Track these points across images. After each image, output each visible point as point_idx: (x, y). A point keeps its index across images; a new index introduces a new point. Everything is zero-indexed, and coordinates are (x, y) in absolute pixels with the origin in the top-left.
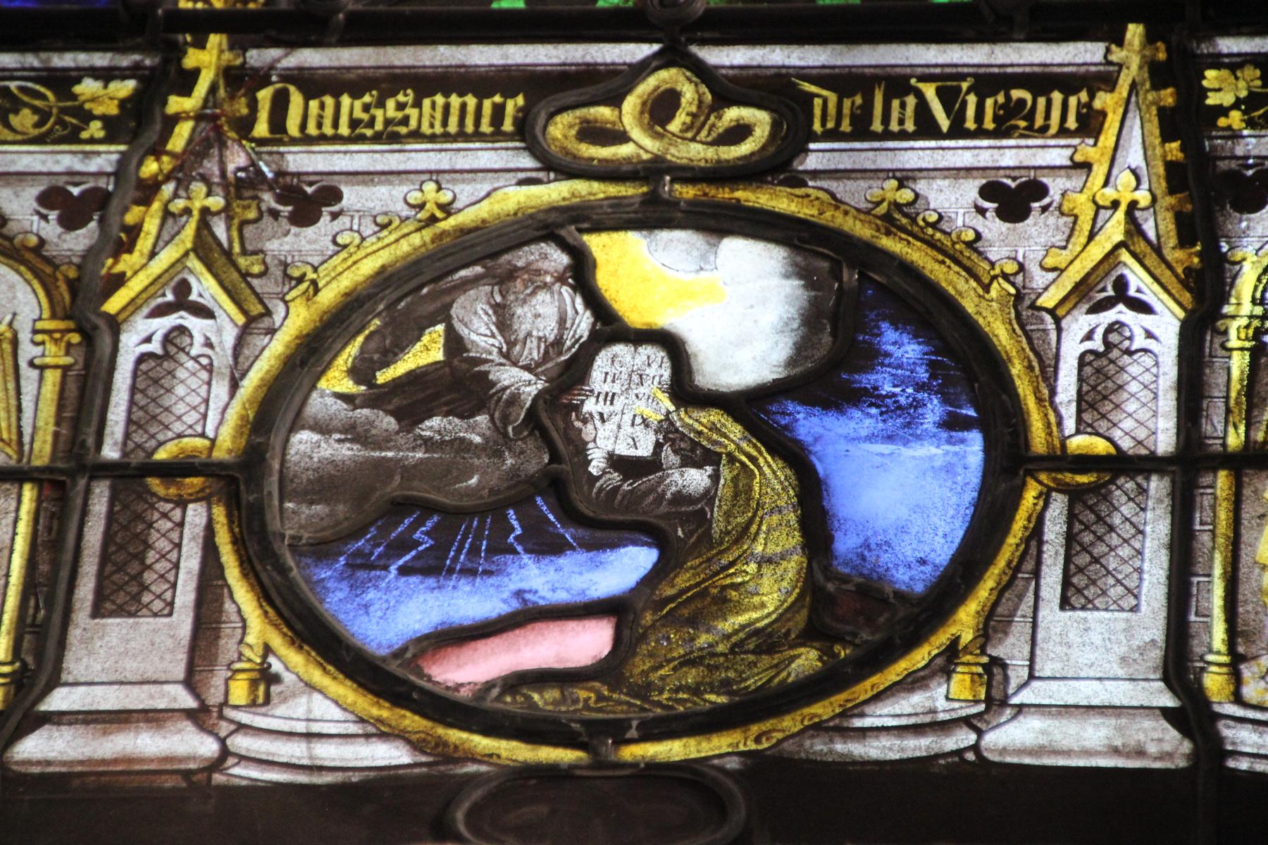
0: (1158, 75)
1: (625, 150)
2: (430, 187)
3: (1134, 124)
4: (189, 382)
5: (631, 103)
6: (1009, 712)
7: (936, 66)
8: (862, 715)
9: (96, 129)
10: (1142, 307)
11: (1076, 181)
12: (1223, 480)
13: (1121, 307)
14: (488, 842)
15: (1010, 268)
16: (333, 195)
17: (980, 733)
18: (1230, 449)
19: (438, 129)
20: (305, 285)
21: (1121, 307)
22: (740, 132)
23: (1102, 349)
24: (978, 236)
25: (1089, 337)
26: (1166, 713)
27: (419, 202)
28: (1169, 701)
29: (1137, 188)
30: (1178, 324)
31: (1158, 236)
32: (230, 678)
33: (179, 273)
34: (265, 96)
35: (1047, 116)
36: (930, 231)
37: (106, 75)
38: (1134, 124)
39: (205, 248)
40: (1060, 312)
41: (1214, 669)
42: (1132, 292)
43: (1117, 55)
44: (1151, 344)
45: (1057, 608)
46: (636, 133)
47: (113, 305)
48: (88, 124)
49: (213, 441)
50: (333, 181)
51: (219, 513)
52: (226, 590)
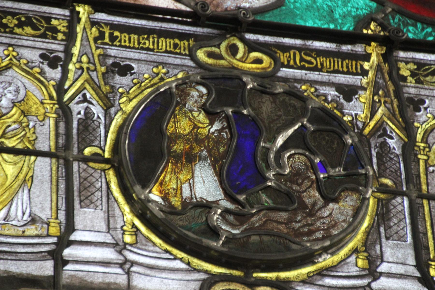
1: (222, 62)
7: (106, 20)
8: (333, 271)
14: (34, 287)
22: (258, 61)
34: (292, 52)
35: (162, 46)
50: (424, 98)
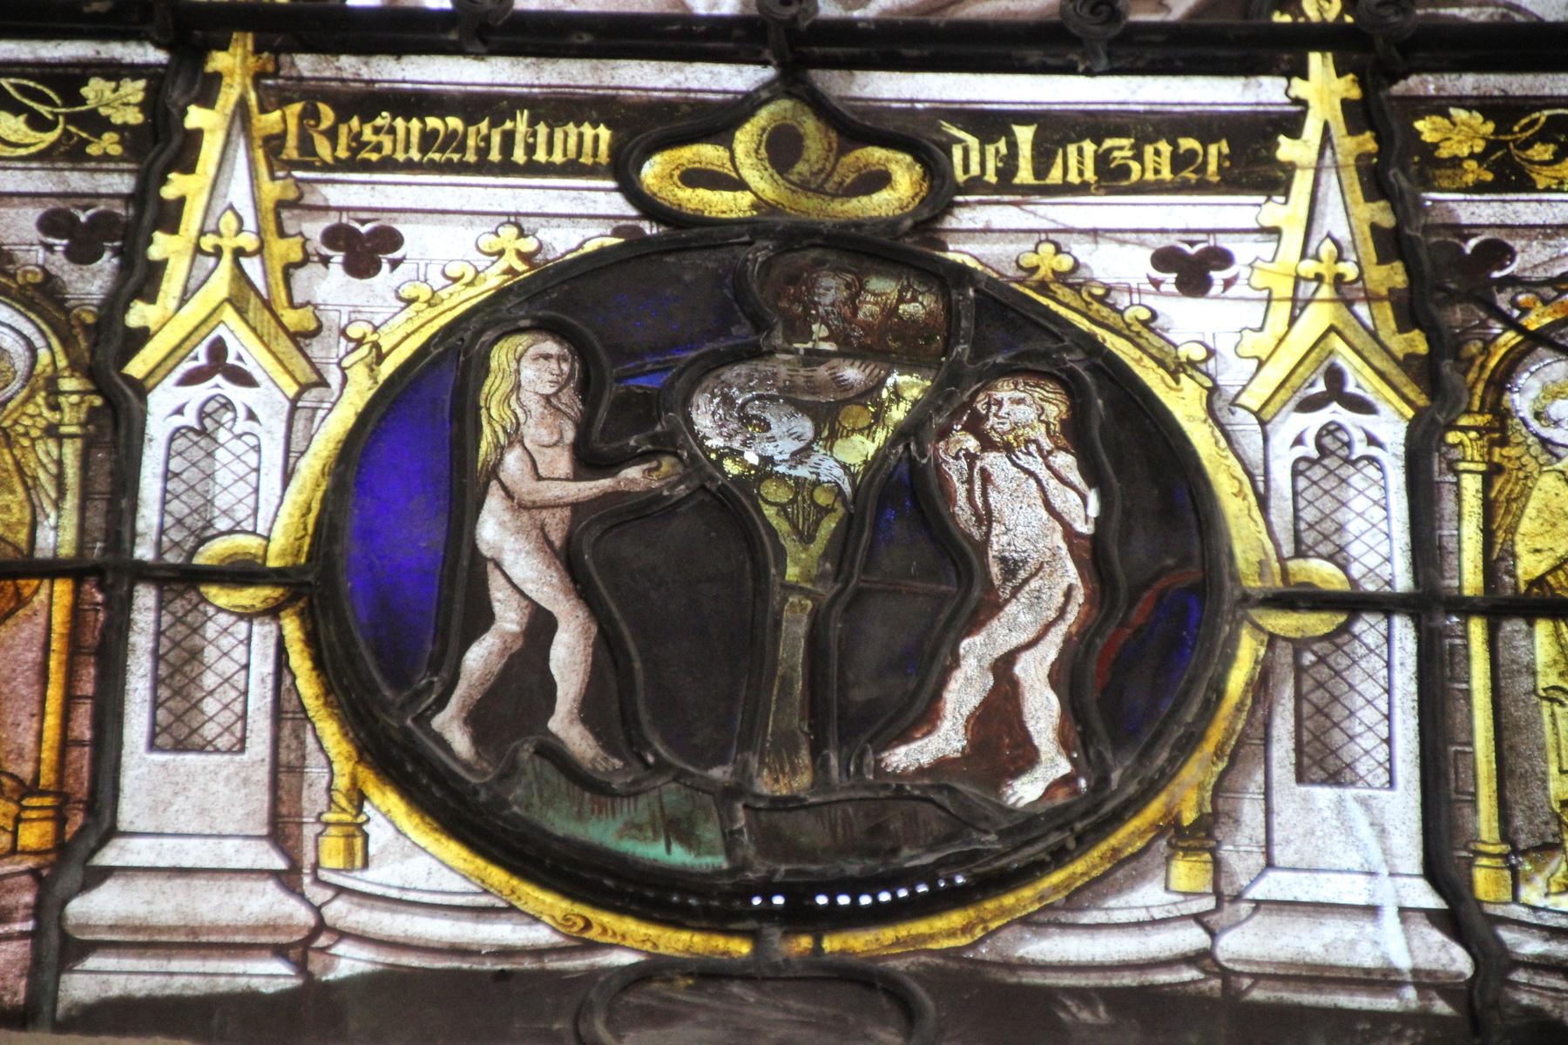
0: (1357, 115)
2: (510, 232)
3: (1330, 180)
4: (201, 464)
5: (746, 138)
6: (1245, 908)
9: (109, 143)
10: (1360, 405)
11: (1266, 248)
12: (1477, 630)
13: (218, 379)
15: (1198, 353)
16: (390, 240)
17: (1213, 934)
18: (38, 555)
19: (558, 158)
20: (364, 350)
21: (1335, 406)
23: (1315, 454)
24: (1154, 316)
25: (1299, 441)
26: (1432, 917)
27: (496, 249)
28: (1432, 901)
29: (240, 230)
30: (1404, 425)
31: (269, 293)
32: (320, 834)
33: (212, 330)
36: (1096, 306)
37: (114, 71)
38: (1330, 180)
39: (241, 296)
40: (1266, 415)
41: (1484, 861)
42: (1350, 388)
43: (1299, 88)
44: (1374, 451)
45: (1293, 784)
46: (751, 175)
47: (137, 367)
48: (99, 136)
49: (268, 539)
51: (292, 628)
52: (309, 726)
